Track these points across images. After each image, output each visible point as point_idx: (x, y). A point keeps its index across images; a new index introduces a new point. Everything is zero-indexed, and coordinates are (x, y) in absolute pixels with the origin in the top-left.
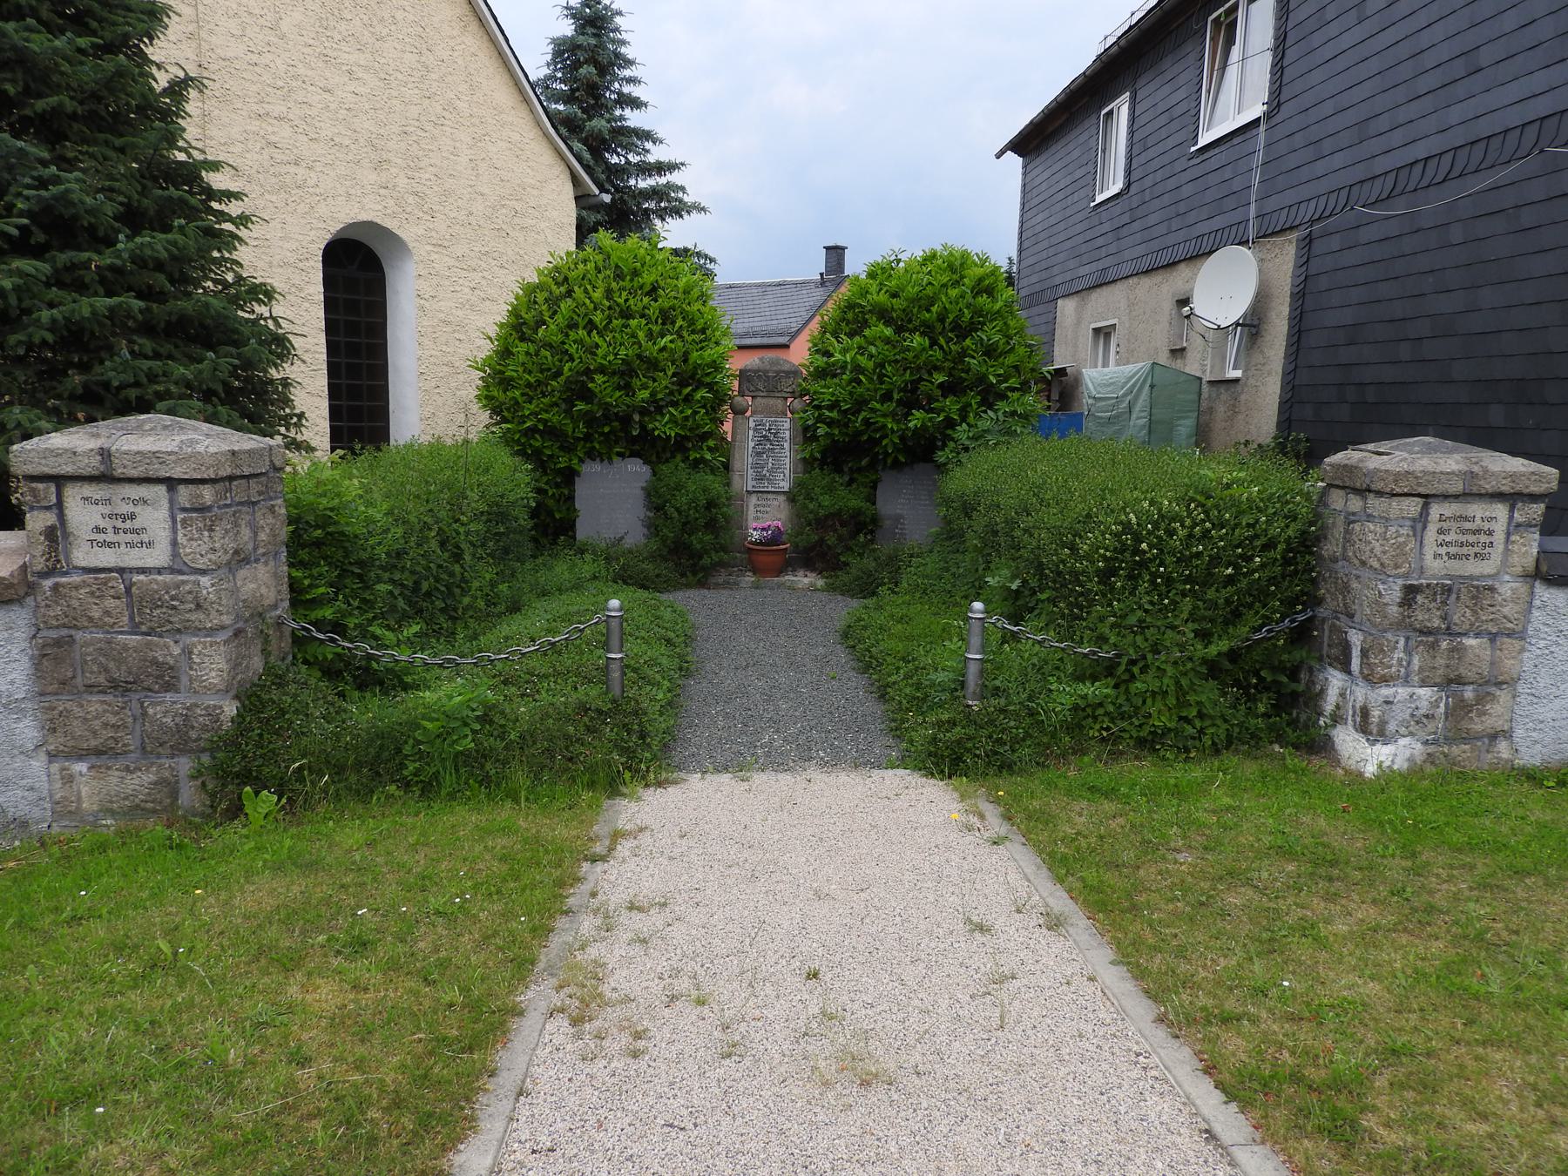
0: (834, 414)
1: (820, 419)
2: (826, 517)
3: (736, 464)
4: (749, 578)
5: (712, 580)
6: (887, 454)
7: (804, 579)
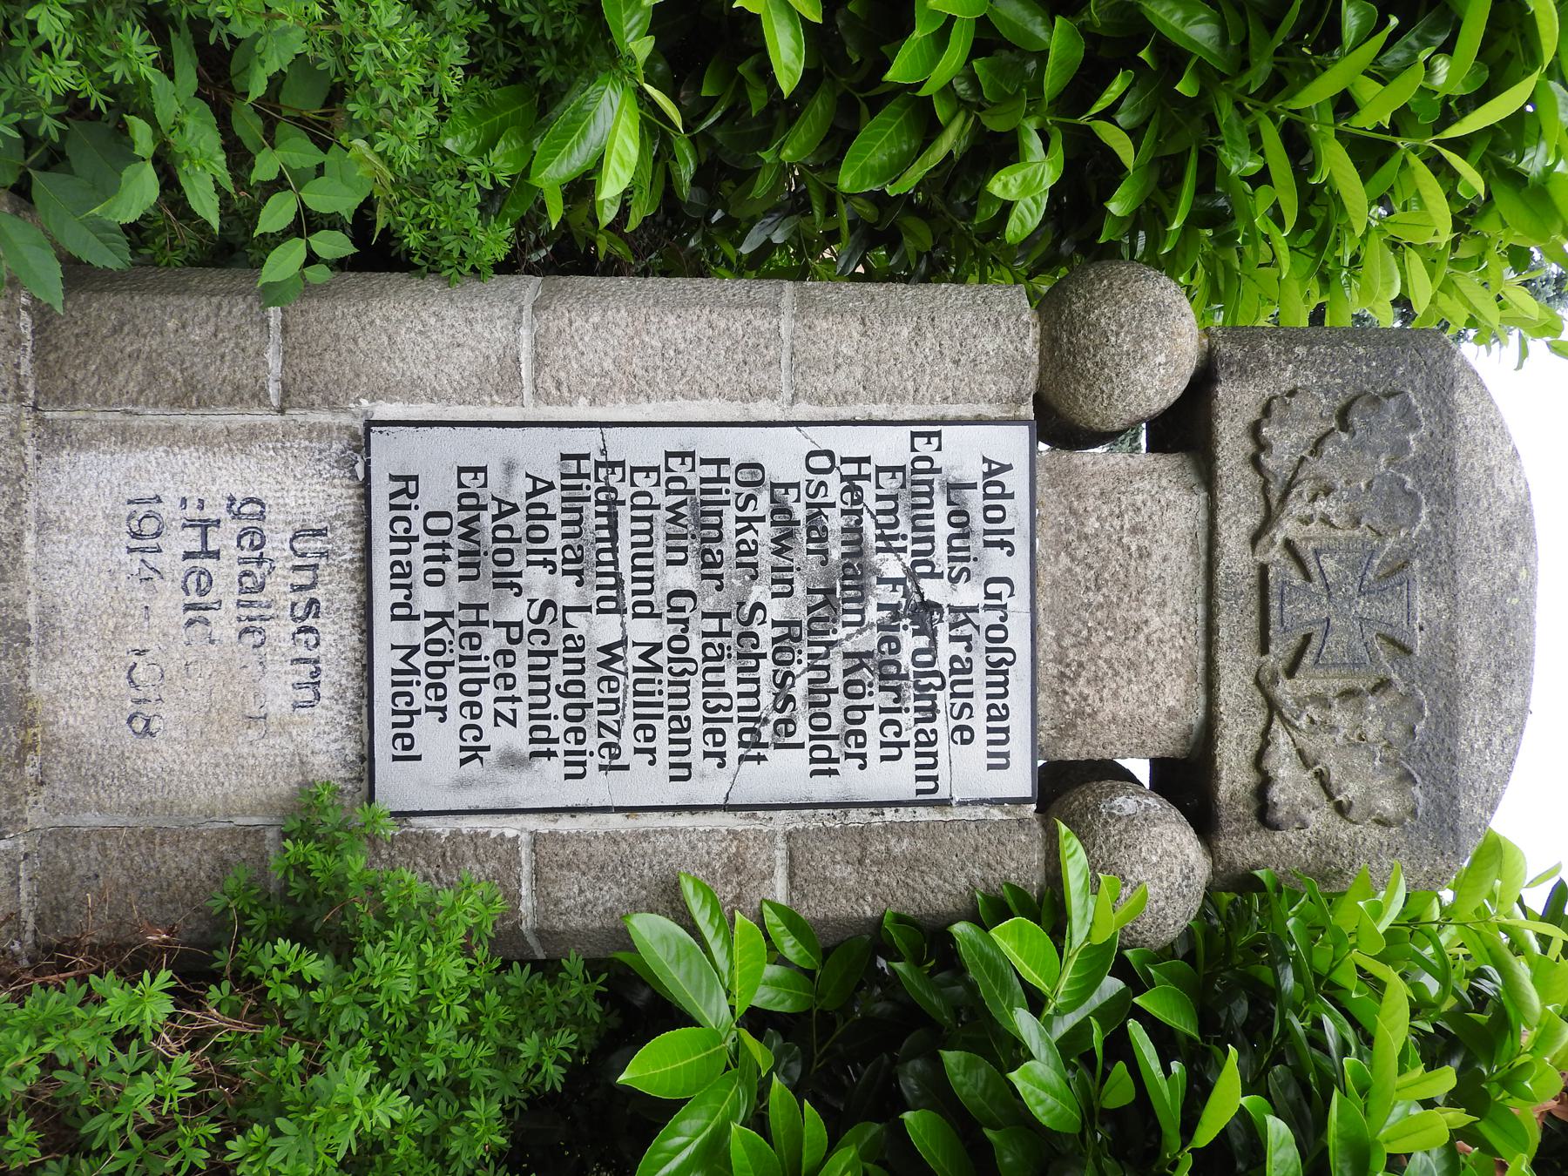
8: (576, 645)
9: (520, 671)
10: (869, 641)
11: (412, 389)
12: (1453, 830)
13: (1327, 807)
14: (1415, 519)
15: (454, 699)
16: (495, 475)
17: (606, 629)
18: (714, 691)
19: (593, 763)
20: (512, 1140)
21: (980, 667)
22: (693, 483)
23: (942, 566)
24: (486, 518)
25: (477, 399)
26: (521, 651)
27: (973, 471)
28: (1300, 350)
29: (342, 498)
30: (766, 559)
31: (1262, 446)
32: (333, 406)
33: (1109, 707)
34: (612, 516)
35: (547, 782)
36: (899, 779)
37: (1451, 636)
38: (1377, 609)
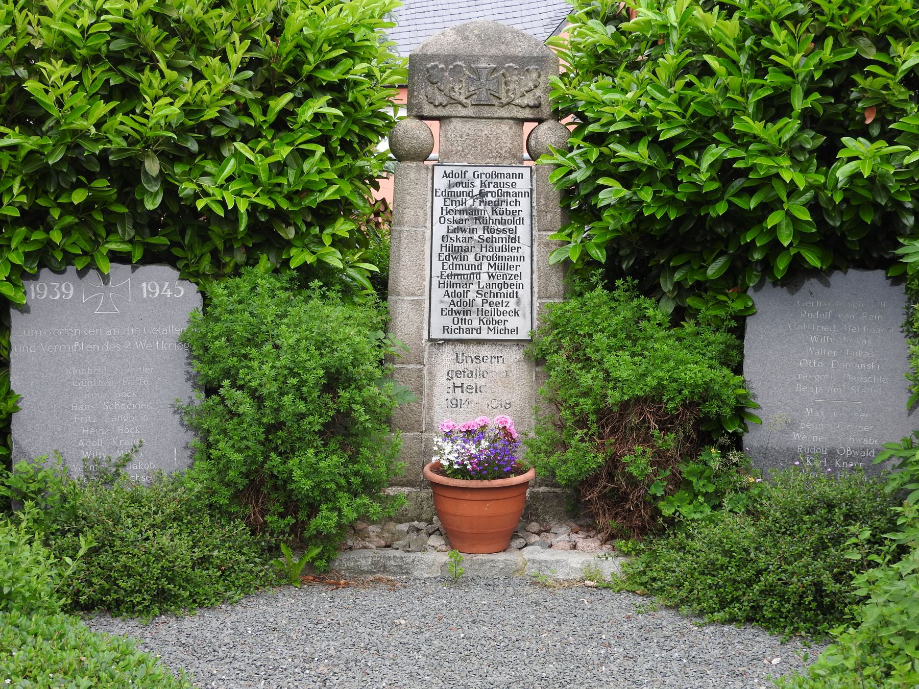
0: (641, 154)
1: (603, 167)
2: (624, 406)
3: (404, 277)
4: (435, 557)
5: (344, 561)
6: (775, 247)
7: (571, 557)
8: (489, 285)
9: (495, 300)
10: (489, 208)
11: (420, 329)
12: (542, 58)
13: (535, 90)
14: (461, 66)
15: (502, 318)
16: (443, 306)
17: (484, 277)
18: (501, 249)
19: (519, 281)
20: (30, 208)
21: (496, 180)
22: (447, 253)
23: (470, 189)
24: (455, 308)
25: (423, 311)
26: (490, 300)
27: (446, 180)
28: (415, 94)
29: (448, 350)
30: (467, 235)
31: (441, 104)
32: (424, 350)
33: (508, 145)
34: (455, 275)
35: (525, 294)
36: (525, 202)
37: (491, 57)
38: (484, 76)
